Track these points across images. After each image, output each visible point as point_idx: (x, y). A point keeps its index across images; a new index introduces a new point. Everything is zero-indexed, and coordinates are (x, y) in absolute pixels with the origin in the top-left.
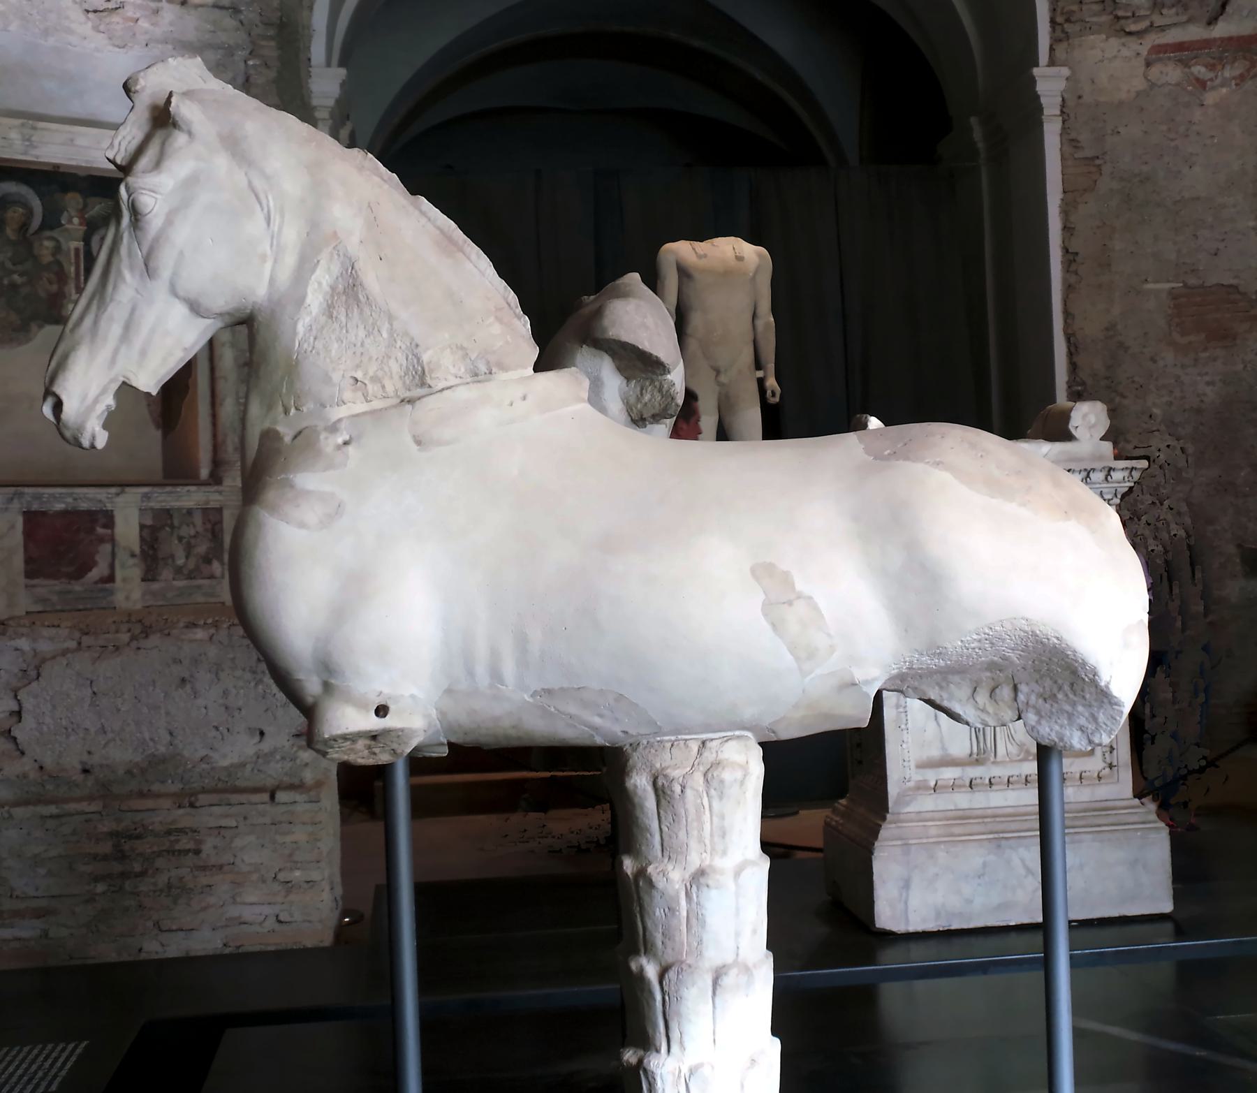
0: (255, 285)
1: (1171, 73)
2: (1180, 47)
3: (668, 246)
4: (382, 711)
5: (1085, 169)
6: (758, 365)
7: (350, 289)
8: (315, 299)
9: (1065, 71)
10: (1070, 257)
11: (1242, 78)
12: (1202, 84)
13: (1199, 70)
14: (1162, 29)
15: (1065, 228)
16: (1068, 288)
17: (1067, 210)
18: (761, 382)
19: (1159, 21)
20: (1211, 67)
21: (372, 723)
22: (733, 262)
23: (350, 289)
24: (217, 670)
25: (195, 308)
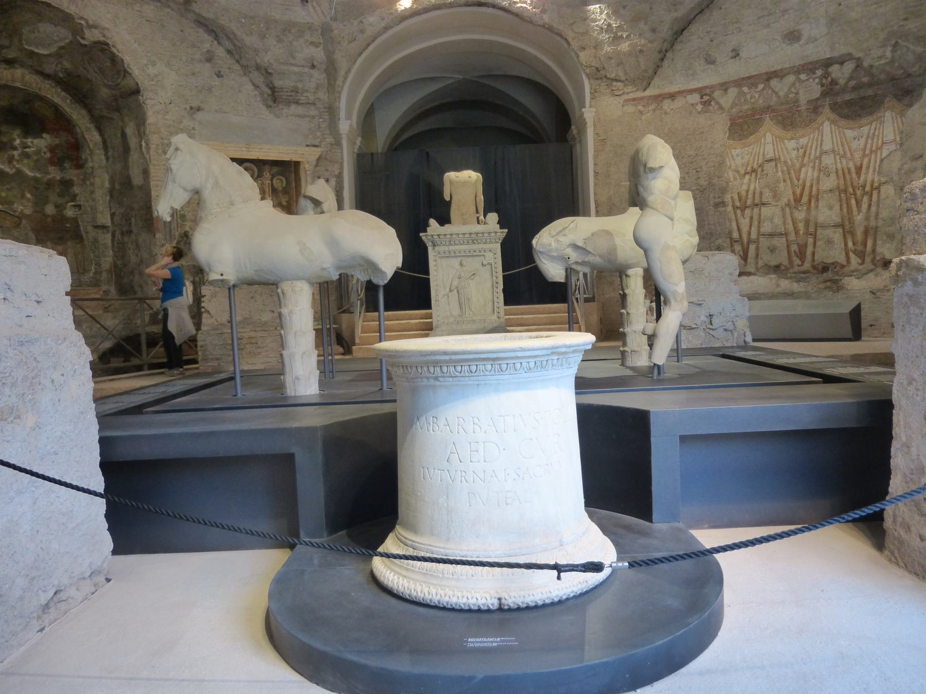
0: (196, 184)
1: (630, 109)
2: (634, 99)
3: (447, 174)
4: (222, 275)
5: (601, 142)
6: (477, 212)
7: (217, 183)
8: (209, 186)
9: (594, 110)
10: (596, 174)
11: (654, 110)
12: (641, 112)
13: (640, 108)
14: (628, 93)
15: (595, 164)
16: (596, 185)
17: (596, 157)
18: (478, 218)
19: (626, 90)
20: (644, 106)
21: (220, 277)
22: (467, 179)
23: (217, 183)
24: (261, 295)
25: (185, 189)
